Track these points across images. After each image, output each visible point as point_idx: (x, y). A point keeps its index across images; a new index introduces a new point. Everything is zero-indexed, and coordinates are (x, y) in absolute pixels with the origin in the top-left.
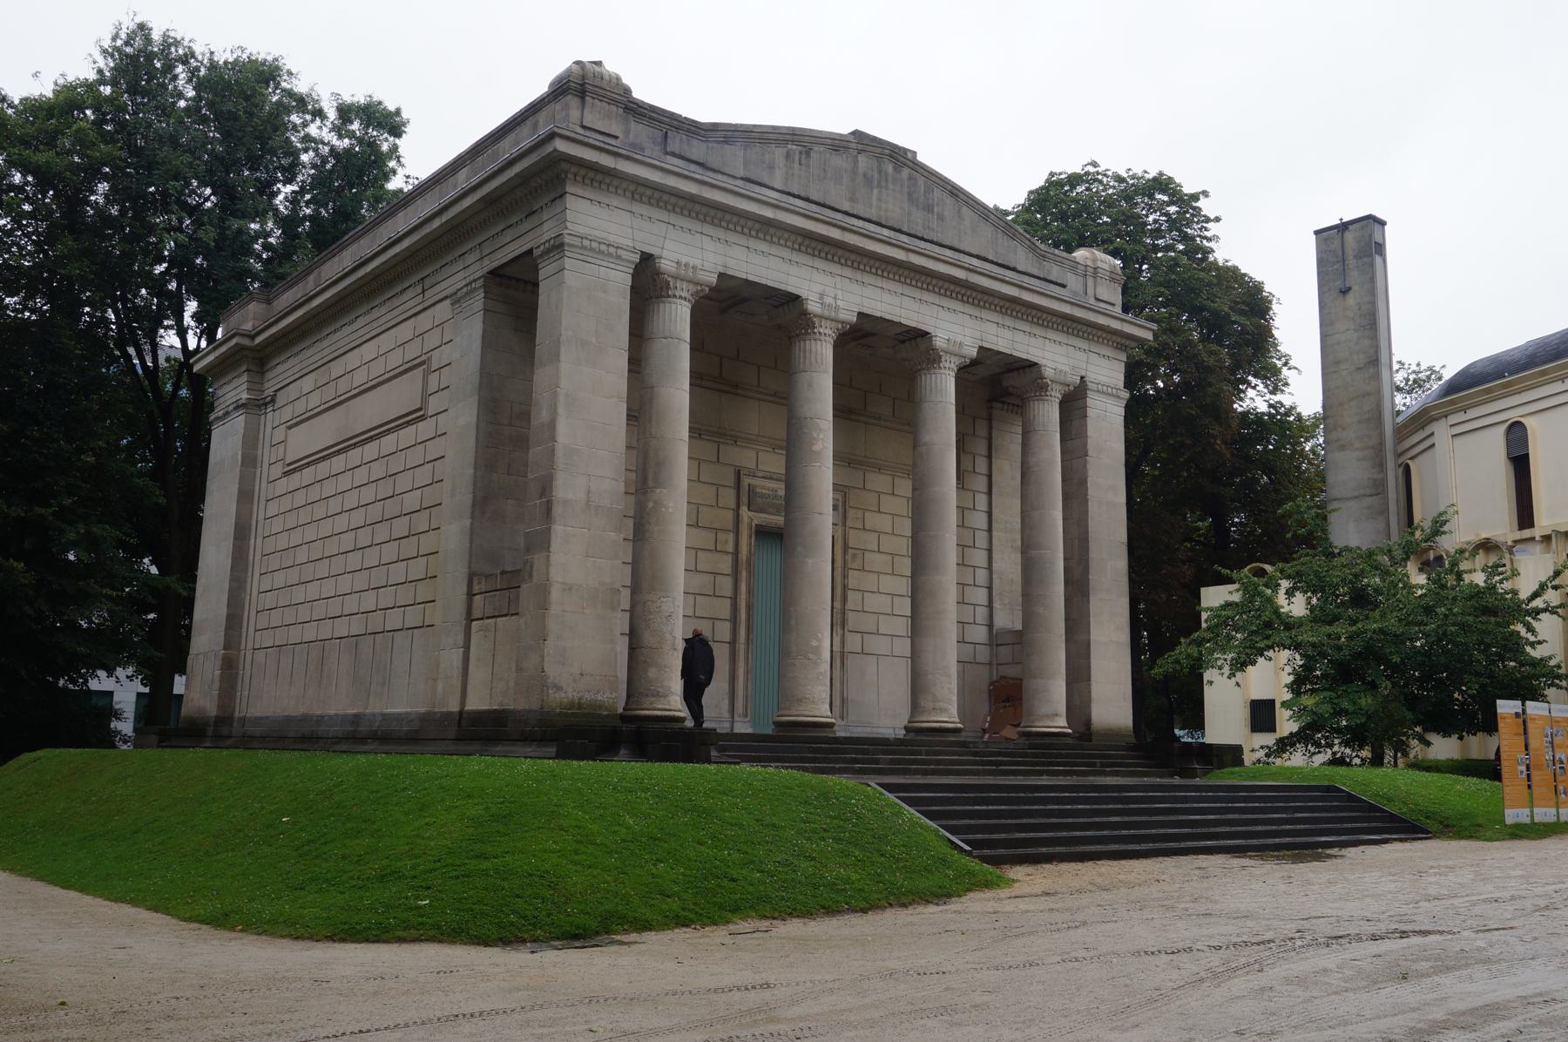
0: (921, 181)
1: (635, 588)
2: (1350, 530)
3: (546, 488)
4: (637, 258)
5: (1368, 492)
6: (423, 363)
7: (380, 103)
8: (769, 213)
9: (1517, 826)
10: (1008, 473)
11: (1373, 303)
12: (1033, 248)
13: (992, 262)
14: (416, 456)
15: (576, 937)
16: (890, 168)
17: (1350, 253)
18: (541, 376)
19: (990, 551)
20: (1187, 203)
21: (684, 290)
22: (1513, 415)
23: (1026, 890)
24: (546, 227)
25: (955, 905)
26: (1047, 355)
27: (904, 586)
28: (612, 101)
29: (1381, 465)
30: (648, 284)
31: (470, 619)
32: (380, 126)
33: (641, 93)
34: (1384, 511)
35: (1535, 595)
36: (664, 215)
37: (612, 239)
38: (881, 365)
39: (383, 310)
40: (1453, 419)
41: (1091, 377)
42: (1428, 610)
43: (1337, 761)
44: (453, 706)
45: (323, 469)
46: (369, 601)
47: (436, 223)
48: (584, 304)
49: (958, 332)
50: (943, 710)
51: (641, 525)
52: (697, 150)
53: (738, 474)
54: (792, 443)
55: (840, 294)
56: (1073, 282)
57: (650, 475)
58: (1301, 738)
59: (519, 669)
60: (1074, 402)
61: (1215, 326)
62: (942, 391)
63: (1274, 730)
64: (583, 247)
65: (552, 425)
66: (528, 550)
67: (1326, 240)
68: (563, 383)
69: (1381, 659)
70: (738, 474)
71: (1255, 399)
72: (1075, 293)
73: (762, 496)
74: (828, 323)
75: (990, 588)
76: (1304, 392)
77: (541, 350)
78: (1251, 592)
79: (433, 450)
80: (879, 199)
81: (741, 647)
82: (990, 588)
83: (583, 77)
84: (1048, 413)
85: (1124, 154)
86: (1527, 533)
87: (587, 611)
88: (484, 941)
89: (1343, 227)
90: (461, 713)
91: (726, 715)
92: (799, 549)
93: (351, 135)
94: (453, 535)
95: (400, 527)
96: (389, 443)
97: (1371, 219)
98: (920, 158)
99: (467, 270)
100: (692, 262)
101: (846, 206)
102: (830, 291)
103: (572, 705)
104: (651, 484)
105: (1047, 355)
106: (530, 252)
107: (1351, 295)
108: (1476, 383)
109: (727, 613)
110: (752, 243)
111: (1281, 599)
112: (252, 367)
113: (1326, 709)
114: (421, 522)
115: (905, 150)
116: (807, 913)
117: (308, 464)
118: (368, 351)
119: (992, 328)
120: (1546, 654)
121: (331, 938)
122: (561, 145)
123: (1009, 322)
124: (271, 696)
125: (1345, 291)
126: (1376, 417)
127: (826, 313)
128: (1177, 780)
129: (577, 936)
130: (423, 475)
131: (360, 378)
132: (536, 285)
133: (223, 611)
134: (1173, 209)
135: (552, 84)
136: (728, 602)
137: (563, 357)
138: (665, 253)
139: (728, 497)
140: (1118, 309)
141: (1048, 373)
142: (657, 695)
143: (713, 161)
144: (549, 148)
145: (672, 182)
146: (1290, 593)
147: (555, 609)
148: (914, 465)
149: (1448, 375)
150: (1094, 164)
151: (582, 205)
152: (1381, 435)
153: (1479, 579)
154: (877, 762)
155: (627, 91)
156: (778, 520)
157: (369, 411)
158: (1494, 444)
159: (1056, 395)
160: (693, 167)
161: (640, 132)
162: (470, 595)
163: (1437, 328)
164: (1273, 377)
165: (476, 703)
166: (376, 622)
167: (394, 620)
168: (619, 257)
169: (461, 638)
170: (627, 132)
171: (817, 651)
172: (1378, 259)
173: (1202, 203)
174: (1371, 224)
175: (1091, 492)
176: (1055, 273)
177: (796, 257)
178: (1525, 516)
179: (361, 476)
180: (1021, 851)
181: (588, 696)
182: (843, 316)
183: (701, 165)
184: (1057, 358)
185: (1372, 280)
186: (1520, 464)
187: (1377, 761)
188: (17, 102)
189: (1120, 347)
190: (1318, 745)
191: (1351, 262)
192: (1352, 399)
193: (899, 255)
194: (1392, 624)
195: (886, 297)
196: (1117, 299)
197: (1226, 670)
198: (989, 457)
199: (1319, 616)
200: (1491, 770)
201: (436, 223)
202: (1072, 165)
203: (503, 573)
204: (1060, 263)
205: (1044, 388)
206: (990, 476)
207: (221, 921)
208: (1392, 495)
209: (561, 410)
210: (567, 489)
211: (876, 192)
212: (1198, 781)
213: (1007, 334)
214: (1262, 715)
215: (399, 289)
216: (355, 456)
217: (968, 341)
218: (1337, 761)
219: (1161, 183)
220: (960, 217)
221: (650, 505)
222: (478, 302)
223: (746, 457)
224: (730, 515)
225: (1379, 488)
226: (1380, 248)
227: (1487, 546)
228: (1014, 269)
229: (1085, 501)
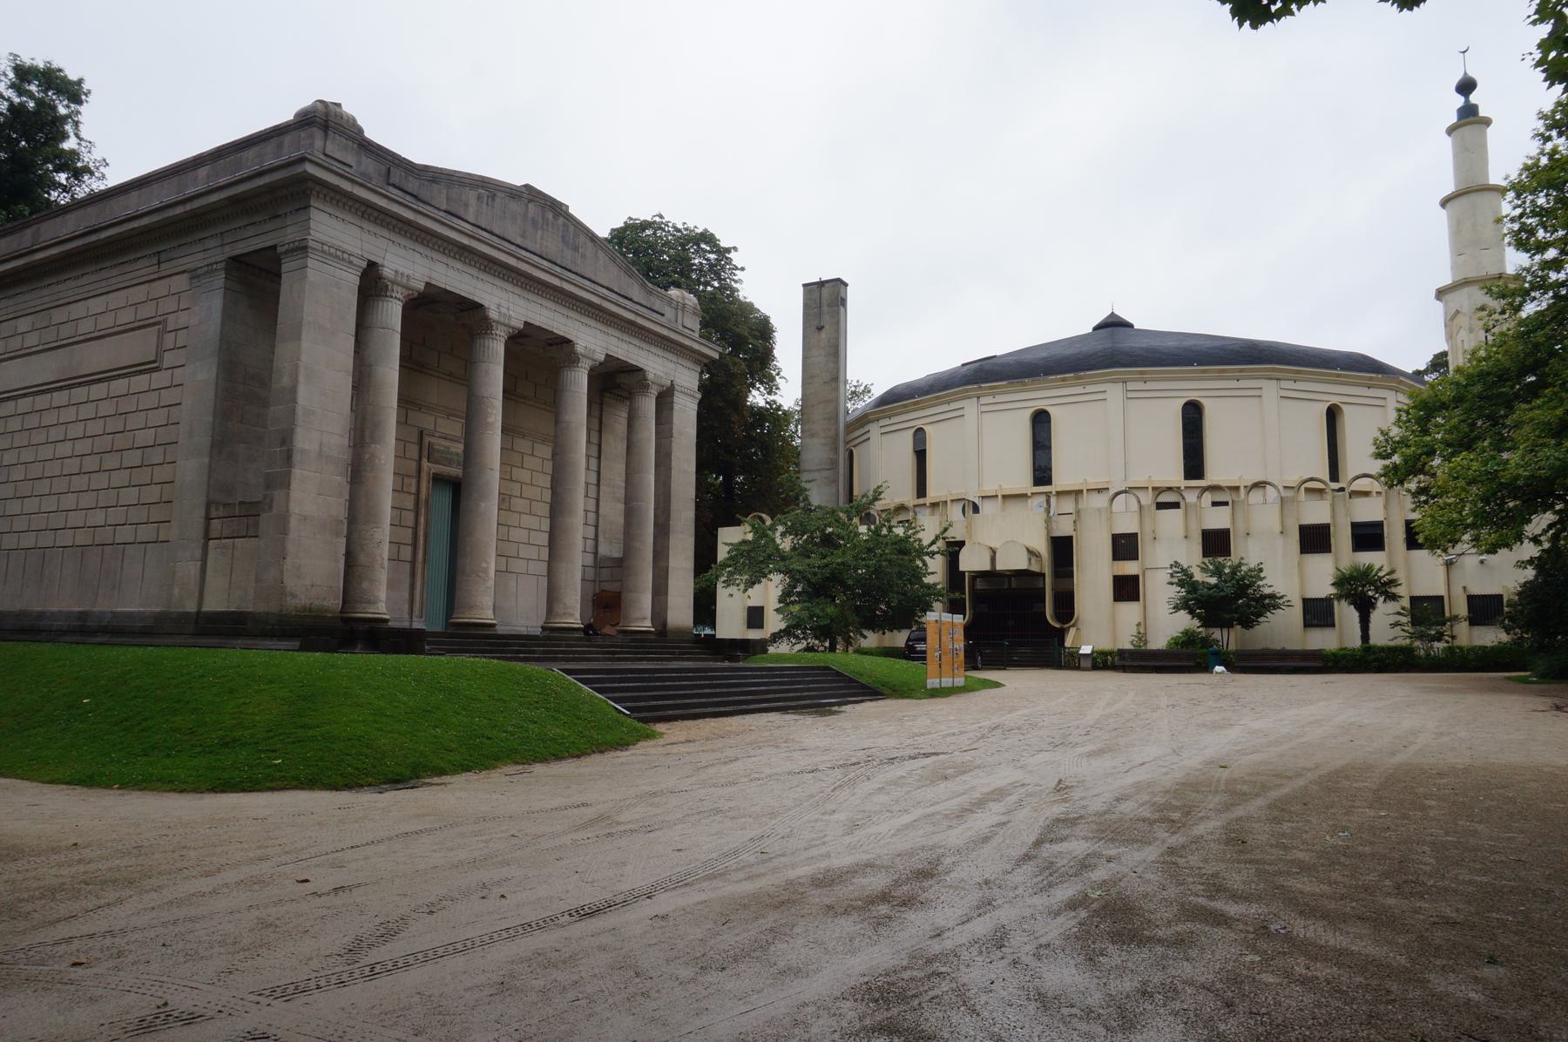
0: (572, 228)
1: (352, 519)
2: (818, 495)
3: (286, 439)
4: (364, 264)
6: (158, 323)
7: (60, 70)
8: (465, 241)
9: (933, 689)
10: (615, 444)
11: (837, 339)
12: (644, 286)
14: (150, 400)
15: (397, 781)
16: (550, 216)
17: (825, 302)
18: (283, 350)
19: (598, 500)
20: (723, 252)
21: (399, 293)
22: (918, 423)
23: (674, 739)
24: (289, 230)
25: (632, 750)
28: (348, 138)
29: (836, 450)
30: (372, 284)
31: (207, 538)
32: (59, 92)
33: (369, 134)
34: (836, 481)
35: (933, 543)
36: (385, 233)
37: (345, 246)
38: (538, 359)
39: (114, 272)
40: (882, 422)
41: (677, 381)
42: (869, 550)
43: (809, 649)
44: (191, 607)
45: (42, 401)
46: (98, 518)
47: (179, 210)
48: (320, 298)
49: (593, 342)
50: (571, 615)
51: (358, 471)
52: (412, 185)
53: (421, 433)
54: (471, 417)
57: (367, 433)
58: (787, 633)
59: (258, 580)
60: (665, 398)
61: (737, 343)
62: (579, 383)
63: (761, 627)
65: (293, 390)
66: (268, 487)
68: (304, 357)
69: (842, 583)
70: (421, 433)
71: (757, 398)
75: (597, 527)
76: (788, 393)
77: (281, 328)
78: (760, 532)
79: (168, 397)
81: (419, 566)
82: (597, 527)
83: (327, 114)
84: (648, 405)
85: (684, 215)
86: (921, 501)
88: (335, 788)
89: (821, 284)
90: (198, 613)
91: (406, 616)
93: (31, 95)
94: (190, 469)
95: (133, 458)
96: (119, 386)
97: (839, 280)
98: (571, 211)
99: (212, 252)
100: (407, 272)
101: (519, 241)
103: (304, 609)
106: (274, 247)
108: (898, 399)
109: (409, 540)
110: (451, 262)
111: (778, 541)
113: (805, 614)
114: (156, 456)
115: (562, 204)
116: (544, 760)
117: (8, 399)
118: (96, 305)
119: (614, 341)
121: (214, 790)
122: (311, 169)
123: (626, 337)
125: (820, 328)
126: (835, 418)
128: (727, 664)
129: (397, 781)
130: (158, 417)
131: (85, 327)
132: (279, 276)
134: (712, 256)
135: (297, 115)
136: (410, 531)
139: (413, 451)
140: (697, 335)
141: (650, 376)
142: (369, 602)
143: (423, 194)
144: (299, 169)
145: (395, 208)
146: (783, 535)
147: (293, 535)
148: (556, 437)
149: (878, 391)
150: (661, 216)
151: (323, 217)
152: (837, 430)
153: (900, 531)
154: (533, 652)
155: (361, 131)
156: (455, 471)
157: (97, 357)
158: (906, 441)
159: (654, 392)
160: (408, 198)
161: (369, 165)
162: (208, 519)
163: (877, 362)
164: (770, 384)
165: (213, 604)
167: (125, 534)
169: (198, 553)
170: (359, 163)
171: (486, 571)
173: (732, 255)
174: (839, 284)
176: (658, 305)
177: (482, 276)
178: (921, 490)
179: (87, 411)
180: (656, 714)
181: (317, 603)
182: (514, 323)
183: (415, 197)
184: (656, 365)
185: (838, 323)
186: (921, 455)
187: (832, 649)
188: (1333, 590)
189: (697, 362)
190: (796, 637)
191: (825, 309)
193: (556, 282)
194: (848, 558)
195: (545, 312)
196: (697, 327)
197: (742, 587)
198: (600, 431)
199: (802, 552)
200: (911, 653)
201: (179, 210)
202: (645, 215)
204: (661, 298)
205: (646, 387)
206: (600, 446)
207: (90, 781)
208: (841, 471)
209: (301, 379)
210: (305, 440)
212: (741, 664)
213: (625, 346)
214: (755, 617)
215: (132, 257)
216: (80, 394)
217: (598, 349)
218: (809, 649)
219: (707, 237)
222: (219, 280)
223: (427, 421)
224: (414, 464)
225: (834, 464)
226: (843, 302)
227: (901, 508)
229: (669, 469)
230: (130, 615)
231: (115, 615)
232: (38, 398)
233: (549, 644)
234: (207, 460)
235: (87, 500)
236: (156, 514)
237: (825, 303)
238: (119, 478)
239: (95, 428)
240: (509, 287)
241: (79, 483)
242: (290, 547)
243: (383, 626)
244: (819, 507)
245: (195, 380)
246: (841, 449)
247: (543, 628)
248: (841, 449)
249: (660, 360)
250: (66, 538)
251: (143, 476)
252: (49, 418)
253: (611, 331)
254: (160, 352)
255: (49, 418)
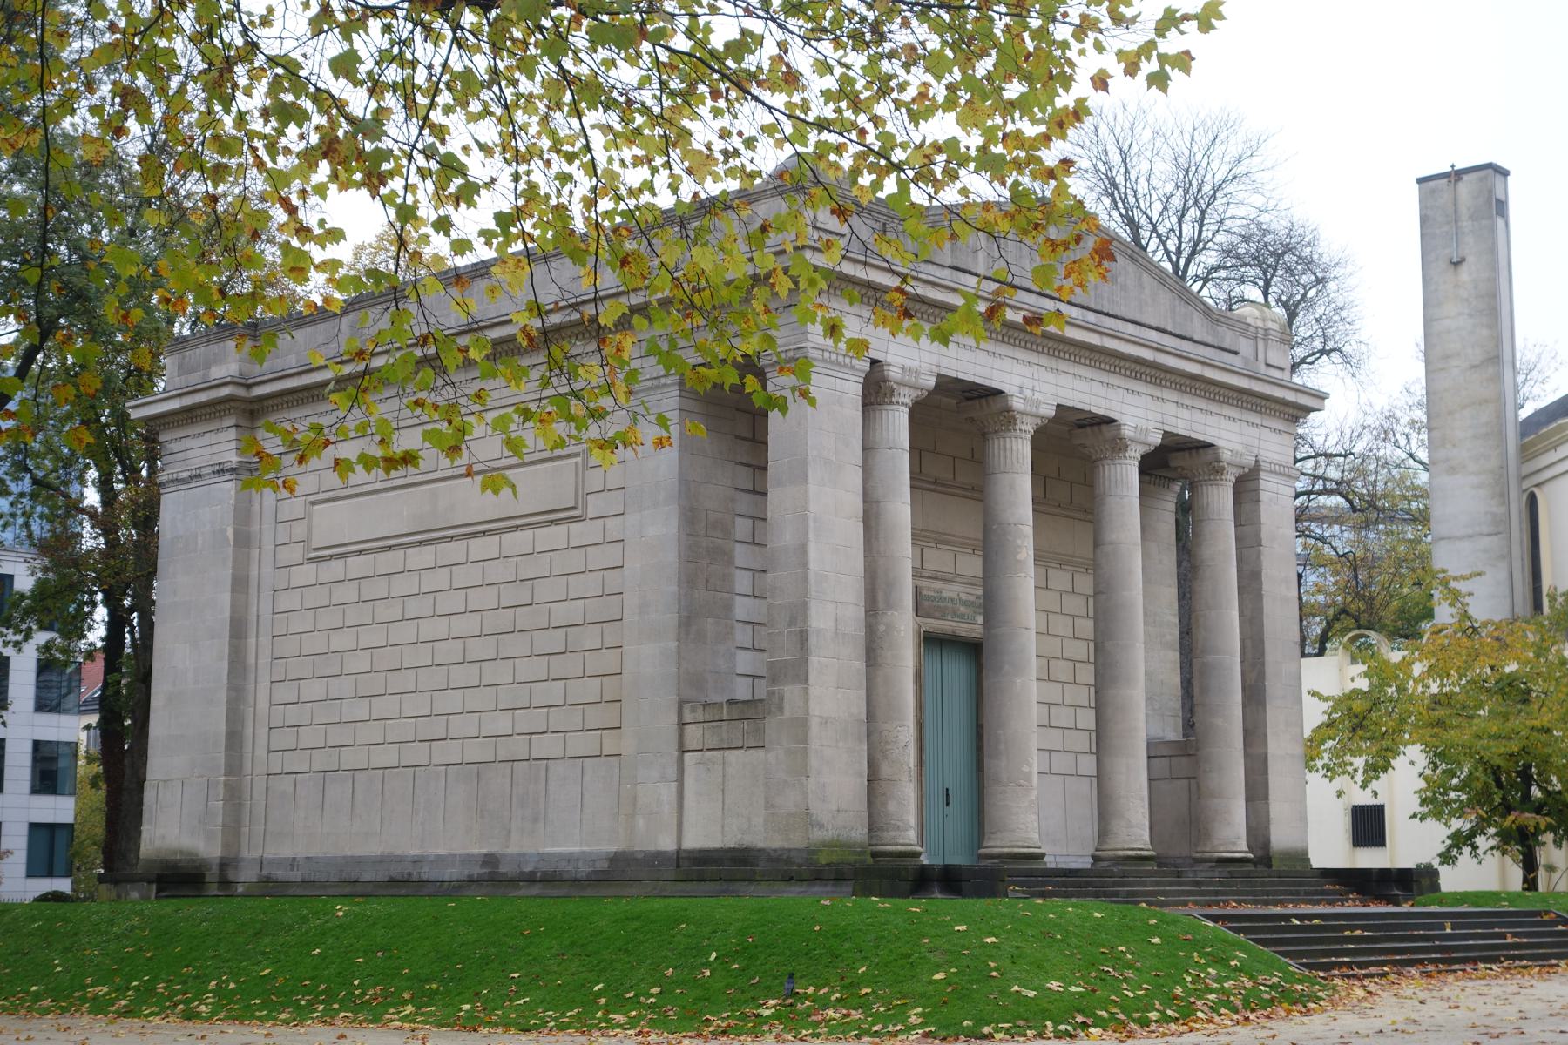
5: (1486, 530)
11: (1493, 281)
13: (1170, 333)
17: (1464, 212)
26: (1224, 434)
27: (1084, 696)
30: (876, 389)
41: (1264, 455)
44: (667, 844)
45: (387, 561)
46: (502, 723)
49: (1143, 416)
56: (1245, 346)
59: (769, 805)
60: (1246, 486)
64: (824, 360)
65: (802, 549)
67: (1433, 191)
68: (813, 507)
72: (1245, 359)
73: (928, 598)
84: (1220, 499)
89: (1456, 175)
90: (678, 852)
92: (1007, 667)
94: (649, 657)
95: (555, 641)
102: (1028, 383)
104: (881, 605)
105: (1224, 434)
107: (1464, 268)
112: (242, 422)
114: (590, 638)
120: (371, 31)
123: (1188, 400)
124: (305, 832)
127: (1028, 409)
128: (1391, 909)
133: (222, 728)
137: (810, 480)
138: (890, 359)
141: (1226, 456)
147: (815, 743)
156: (971, 628)
159: (1230, 477)
162: (682, 724)
165: (695, 839)
166: (518, 747)
167: (547, 746)
169: (672, 772)
172: (1500, 222)
175: (1267, 586)
185: (1493, 250)
191: (1466, 224)
192: (1464, 407)
193: (1094, 339)
203: (731, 702)
209: (811, 536)
210: (820, 619)
213: (1185, 413)
214: (1368, 825)
220: (1141, 286)
221: (882, 628)
226: (1501, 207)
230: (570, 858)
231: (543, 858)
232: (381, 557)
233: (1106, 878)
234: (673, 645)
235: (477, 700)
236: (595, 717)
237: (1465, 212)
238: (526, 669)
239: (488, 598)
240: (1033, 357)
241: (460, 675)
242: (814, 762)
243: (909, 861)
244: (1485, 624)
245: (653, 533)
246: (1514, 494)
247: (1096, 859)
248: (1514, 494)
249: (1235, 426)
250: (451, 752)
251: (571, 665)
252: (401, 586)
253: (1168, 394)
254: (582, 494)
255: (401, 586)
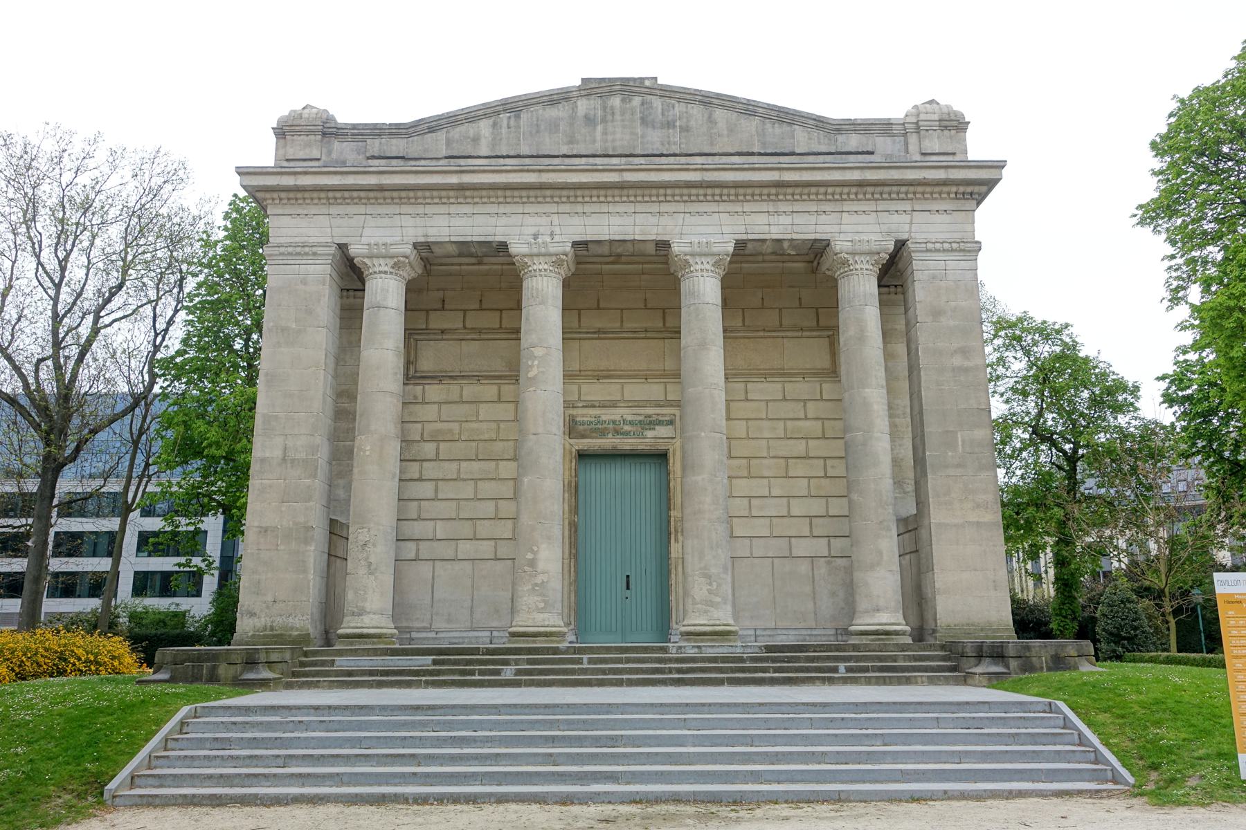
21: (382, 265)
33: (345, 116)
55: (557, 230)
73: (584, 423)
74: (542, 259)
80: (605, 133)
87: (282, 547)
101: (565, 150)
127: (535, 251)
160: (394, 162)
168: (315, 254)
211: (599, 128)
228: (753, 154)
